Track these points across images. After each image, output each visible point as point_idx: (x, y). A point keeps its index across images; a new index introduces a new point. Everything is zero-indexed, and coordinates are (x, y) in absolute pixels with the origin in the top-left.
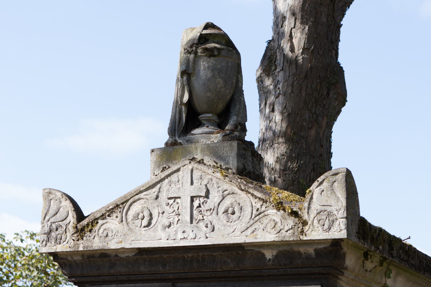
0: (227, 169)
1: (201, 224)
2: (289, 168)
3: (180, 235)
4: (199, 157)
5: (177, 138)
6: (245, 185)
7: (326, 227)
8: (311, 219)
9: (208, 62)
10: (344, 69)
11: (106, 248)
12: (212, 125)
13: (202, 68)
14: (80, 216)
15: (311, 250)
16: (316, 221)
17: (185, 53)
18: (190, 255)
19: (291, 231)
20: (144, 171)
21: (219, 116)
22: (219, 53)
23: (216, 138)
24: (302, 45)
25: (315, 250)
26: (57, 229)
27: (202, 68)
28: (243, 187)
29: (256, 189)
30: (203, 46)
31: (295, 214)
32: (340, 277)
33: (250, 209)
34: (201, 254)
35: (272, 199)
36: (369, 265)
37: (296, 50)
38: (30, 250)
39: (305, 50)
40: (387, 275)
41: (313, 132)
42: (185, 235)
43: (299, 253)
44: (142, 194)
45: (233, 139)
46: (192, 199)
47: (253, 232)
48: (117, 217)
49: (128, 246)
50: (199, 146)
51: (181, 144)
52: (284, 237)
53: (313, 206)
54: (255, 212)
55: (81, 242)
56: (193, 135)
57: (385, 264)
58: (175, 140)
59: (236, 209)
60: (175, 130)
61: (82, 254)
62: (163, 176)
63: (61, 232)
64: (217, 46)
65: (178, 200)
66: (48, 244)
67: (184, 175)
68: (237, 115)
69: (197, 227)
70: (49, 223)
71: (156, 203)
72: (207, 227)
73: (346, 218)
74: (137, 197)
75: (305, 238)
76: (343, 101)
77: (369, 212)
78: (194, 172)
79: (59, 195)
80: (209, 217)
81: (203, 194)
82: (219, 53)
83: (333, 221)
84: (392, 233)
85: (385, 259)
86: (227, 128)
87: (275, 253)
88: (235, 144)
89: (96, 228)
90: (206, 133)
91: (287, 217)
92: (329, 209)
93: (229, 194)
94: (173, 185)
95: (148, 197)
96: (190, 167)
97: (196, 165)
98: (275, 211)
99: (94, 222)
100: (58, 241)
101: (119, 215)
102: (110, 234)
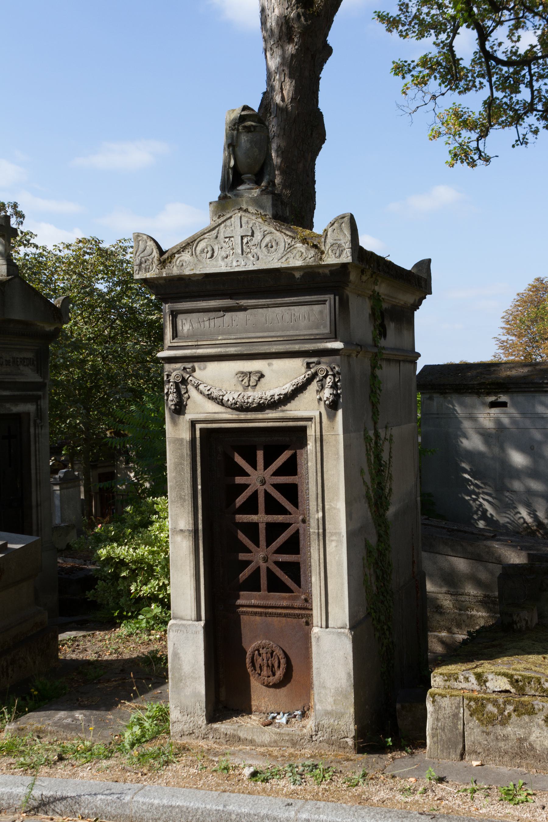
0: (265, 215)
1: (249, 255)
2: (284, 194)
3: (235, 264)
4: (244, 207)
5: (227, 193)
6: (279, 227)
7: (337, 255)
8: (327, 250)
9: (247, 137)
10: (323, 114)
11: (183, 274)
12: (252, 183)
13: (243, 141)
14: (161, 252)
15: (327, 271)
16: (330, 251)
17: (230, 130)
18: (242, 277)
19: (313, 259)
20: (204, 219)
21: (256, 175)
22: (255, 130)
23: (256, 192)
24: (291, 95)
25: (330, 271)
26: (146, 262)
27: (243, 141)
28: (278, 228)
29: (287, 230)
30: (243, 125)
31: (315, 246)
32: (346, 288)
33: (283, 244)
34: (250, 276)
35: (299, 237)
36: (364, 278)
37: (286, 100)
38: (67, 257)
39: (293, 99)
40: (375, 283)
41: (301, 165)
42: (239, 263)
43: (319, 273)
44: (206, 235)
45: (268, 193)
46: (242, 238)
47: (287, 260)
48: (189, 252)
49: (198, 272)
50: (244, 199)
51: (230, 198)
52: (308, 262)
53: (328, 241)
54: (287, 246)
55: (164, 270)
56: (238, 190)
57: (374, 276)
58: (226, 195)
59: (274, 244)
60: (225, 187)
61: (165, 278)
62: (220, 222)
63: (148, 264)
64: (253, 123)
65: (232, 239)
66: (140, 273)
67: (235, 220)
68: (269, 175)
69: (247, 257)
70: (139, 258)
71: (217, 241)
72: (253, 257)
73: (351, 248)
74: (202, 237)
75: (323, 263)
76: (322, 139)
77: (367, 242)
78: (243, 218)
79: (145, 237)
80: (254, 250)
81: (250, 234)
82: (255, 130)
83: (342, 251)
84: (379, 255)
85: (375, 273)
86: (262, 184)
87: (302, 273)
88: (270, 197)
89: (174, 260)
90: (248, 189)
91: (310, 249)
92: (339, 242)
93: (268, 234)
94: (228, 228)
95: (210, 237)
96: (239, 215)
97: (243, 214)
98: (301, 245)
99: (172, 256)
100: (147, 270)
101: (190, 250)
102: (184, 264)
